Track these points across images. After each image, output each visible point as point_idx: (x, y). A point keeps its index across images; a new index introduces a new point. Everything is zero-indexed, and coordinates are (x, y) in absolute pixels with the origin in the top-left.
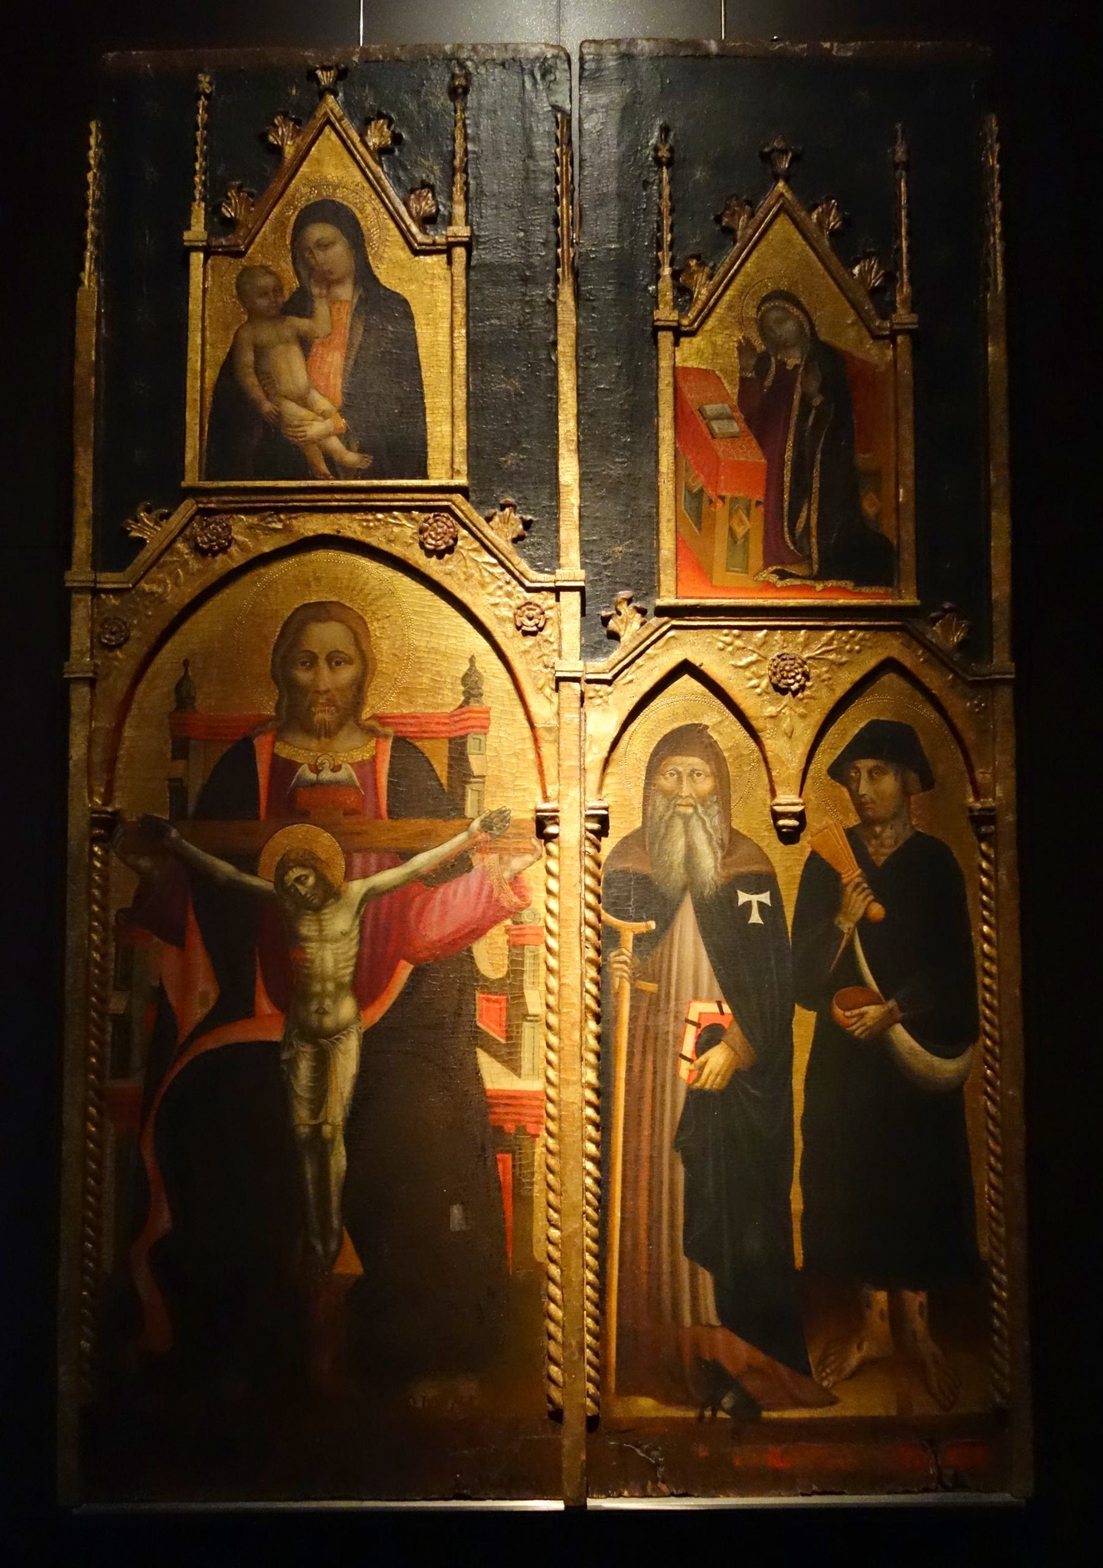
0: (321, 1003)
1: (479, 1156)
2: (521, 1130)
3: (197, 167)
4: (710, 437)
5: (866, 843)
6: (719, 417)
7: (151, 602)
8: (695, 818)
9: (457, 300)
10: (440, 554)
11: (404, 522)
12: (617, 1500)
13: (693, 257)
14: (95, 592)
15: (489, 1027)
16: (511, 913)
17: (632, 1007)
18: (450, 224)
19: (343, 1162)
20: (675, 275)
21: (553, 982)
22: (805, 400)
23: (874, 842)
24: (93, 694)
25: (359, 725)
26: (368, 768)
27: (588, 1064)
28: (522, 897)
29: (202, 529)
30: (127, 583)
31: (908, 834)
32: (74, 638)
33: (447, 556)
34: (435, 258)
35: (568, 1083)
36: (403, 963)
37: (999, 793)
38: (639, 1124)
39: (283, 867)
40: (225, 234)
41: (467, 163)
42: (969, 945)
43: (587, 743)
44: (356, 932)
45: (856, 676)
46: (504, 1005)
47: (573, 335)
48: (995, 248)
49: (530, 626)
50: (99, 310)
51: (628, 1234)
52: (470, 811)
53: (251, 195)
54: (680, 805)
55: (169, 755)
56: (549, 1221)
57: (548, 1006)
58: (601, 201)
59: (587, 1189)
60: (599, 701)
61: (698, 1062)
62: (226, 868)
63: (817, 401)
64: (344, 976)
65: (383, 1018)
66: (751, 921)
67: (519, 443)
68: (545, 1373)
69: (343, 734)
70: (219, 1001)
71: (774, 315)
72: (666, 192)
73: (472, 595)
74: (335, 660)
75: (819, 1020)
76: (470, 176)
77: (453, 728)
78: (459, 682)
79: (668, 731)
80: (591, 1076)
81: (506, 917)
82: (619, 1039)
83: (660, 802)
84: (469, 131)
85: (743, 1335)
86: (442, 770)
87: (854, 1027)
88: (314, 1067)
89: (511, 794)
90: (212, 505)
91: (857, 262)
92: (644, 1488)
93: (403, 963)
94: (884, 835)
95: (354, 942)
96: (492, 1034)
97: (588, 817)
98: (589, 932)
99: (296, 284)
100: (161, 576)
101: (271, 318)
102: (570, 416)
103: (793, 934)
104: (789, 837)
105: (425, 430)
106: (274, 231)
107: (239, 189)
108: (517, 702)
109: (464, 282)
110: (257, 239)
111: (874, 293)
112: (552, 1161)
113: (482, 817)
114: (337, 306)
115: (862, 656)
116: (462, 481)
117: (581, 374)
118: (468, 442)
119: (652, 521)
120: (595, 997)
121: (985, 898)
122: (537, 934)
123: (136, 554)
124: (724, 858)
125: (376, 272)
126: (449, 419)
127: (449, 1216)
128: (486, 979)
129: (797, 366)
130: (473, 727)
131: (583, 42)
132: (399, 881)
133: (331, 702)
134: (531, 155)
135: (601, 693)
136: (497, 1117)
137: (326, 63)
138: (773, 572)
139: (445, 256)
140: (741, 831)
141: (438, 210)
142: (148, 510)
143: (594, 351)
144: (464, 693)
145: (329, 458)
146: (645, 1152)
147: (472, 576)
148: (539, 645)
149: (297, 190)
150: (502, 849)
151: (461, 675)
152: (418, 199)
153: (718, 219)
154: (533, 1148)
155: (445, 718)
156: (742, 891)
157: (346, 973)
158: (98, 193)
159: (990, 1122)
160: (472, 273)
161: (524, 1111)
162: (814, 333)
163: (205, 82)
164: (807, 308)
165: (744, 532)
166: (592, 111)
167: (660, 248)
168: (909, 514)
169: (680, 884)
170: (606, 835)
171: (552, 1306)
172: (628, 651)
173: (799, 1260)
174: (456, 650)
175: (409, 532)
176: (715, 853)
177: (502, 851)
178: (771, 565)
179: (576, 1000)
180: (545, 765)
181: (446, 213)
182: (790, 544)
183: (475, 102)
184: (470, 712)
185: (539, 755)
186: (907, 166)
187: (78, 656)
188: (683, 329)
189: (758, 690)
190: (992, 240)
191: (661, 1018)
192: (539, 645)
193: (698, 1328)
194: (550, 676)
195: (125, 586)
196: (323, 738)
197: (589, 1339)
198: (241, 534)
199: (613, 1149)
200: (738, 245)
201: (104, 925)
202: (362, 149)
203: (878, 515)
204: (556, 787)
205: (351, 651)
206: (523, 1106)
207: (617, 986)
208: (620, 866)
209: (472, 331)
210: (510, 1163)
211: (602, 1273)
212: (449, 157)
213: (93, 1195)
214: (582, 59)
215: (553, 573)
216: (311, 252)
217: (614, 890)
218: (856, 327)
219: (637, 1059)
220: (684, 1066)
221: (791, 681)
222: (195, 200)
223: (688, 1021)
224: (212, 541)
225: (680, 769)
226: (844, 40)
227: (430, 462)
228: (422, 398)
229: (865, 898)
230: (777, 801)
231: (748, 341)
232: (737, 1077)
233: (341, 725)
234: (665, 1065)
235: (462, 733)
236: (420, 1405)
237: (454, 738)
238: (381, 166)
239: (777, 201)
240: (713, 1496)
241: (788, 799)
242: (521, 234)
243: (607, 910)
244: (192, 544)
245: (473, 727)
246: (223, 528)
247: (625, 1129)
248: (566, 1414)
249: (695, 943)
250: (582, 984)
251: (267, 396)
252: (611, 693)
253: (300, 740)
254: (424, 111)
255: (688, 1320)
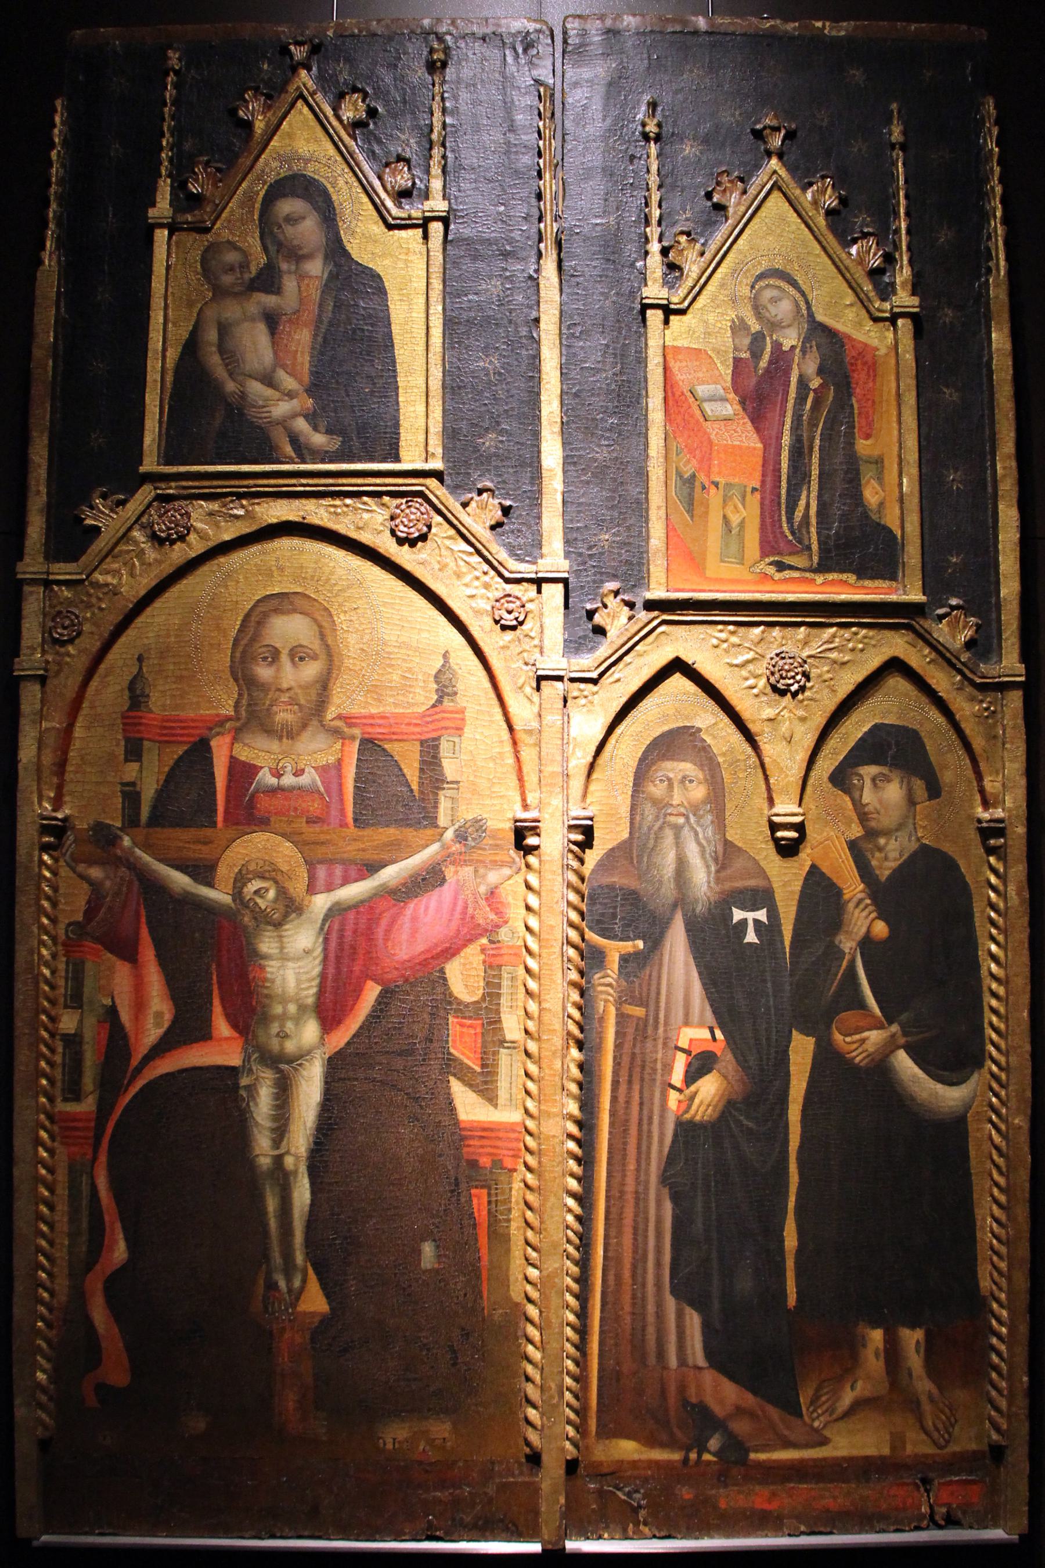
0: (282, 1026)
1: (452, 1191)
2: (498, 1163)
3: (164, 143)
4: (702, 420)
5: (870, 857)
6: (712, 399)
7: (105, 594)
8: (686, 829)
9: (433, 276)
10: (412, 543)
11: (374, 508)
12: (596, 1542)
13: (682, 233)
14: (47, 584)
15: (463, 1054)
16: (486, 931)
17: (617, 1033)
18: (427, 198)
19: (307, 1196)
20: (665, 252)
21: (533, 1007)
22: (803, 383)
23: (877, 854)
24: (43, 693)
25: (323, 726)
26: (333, 772)
27: (570, 1095)
28: (499, 913)
29: (160, 517)
30: (81, 574)
31: (914, 846)
32: (25, 633)
33: (420, 544)
34: (410, 232)
35: (549, 1115)
36: (370, 984)
37: (1008, 804)
38: (624, 1156)
39: (241, 880)
40: (190, 210)
41: (445, 137)
42: (976, 966)
43: (571, 746)
44: (319, 951)
45: (859, 677)
46: (479, 1030)
47: (557, 313)
48: (996, 232)
49: (509, 620)
50: (59, 288)
51: (611, 1278)
52: (443, 820)
53: (218, 170)
54: (670, 814)
55: (122, 757)
56: (527, 1259)
57: (527, 1032)
58: (587, 174)
59: (568, 1227)
60: (583, 701)
61: (688, 1092)
62: (180, 880)
63: (815, 383)
64: (306, 997)
65: (348, 1044)
66: (746, 941)
67: (498, 423)
68: (522, 1371)
69: (306, 735)
70: (175, 1022)
71: (768, 294)
72: (654, 168)
73: (447, 586)
74: (298, 655)
75: (818, 1044)
76: (448, 149)
77: (425, 729)
78: (432, 679)
79: (658, 734)
80: (573, 1108)
81: (481, 935)
82: (603, 1068)
83: (649, 812)
84: (448, 104)
85: (732, 1378)
86: (412, 775)
87: (854, 1054)
88: (273, 1093)
89: (488, 802)
90: (171, 491)
91: (854, 241)
92: (625, 1530)
93: (370, 984)
94: (889, 847)
95: (317, 961)
96: (466, 1061)
97: (571, 828)
98: (572, 952)
99: (263, 260)
100: (116, 566)
101: (236, 295)
102: (553, 396)
103: (790, 953)
104: (788, 850)
105: (398, 410)
106: (242, 205)
107: (207, 164)
108: (495, 702)
109: (441, 257)
110: (224, 215)
111: (875, 274)
112: (531, 1197)
113: (456, 826)
114: (306, 282)
115: (864, 656)
116: (437, 464)
117: (564, 352)
118: (444, 423)
119: (641, 508)
120: (577, 1023)
121: (993, 914)
122: (515, 954)
123: (91, 542)
124: (718, 871)
125: (348, 247)
126: (424, 398)
127: (420, 1254)
128: (460, 1002)
129: (793, 347)
130: (446, 728)
131: (566, 18)
132: (366, 895)
133: (293, 701)
134: (512, 129)
135: (585, 693)
136: (471, 1150)
137: (300, 38)
138: (771, 564)
139: (421, 230)
140: (736, 843)
141: (414, 183)
142: (104, 496)
143: (579, 329)
144: (437, 691)
145: (295, 440)
146: (630, 1187)
147: (446, 565)
148: (519, 640)
149: (266, 164)
150: (478, 861)
151: (434, 673)
152: (394, 174)
153: (709, 196)
154: (510, 1183)
155: (417, 718)
156: (737, 908)
157: (310, 994)
158: (61, 171)
159: (994, 1152)
160: (449, 248)
161: (499, 1143)
162: (811, 315)
163: (174, 58)
164: (804, 287)
165: (739, 520)
166: (576, 85)
167: (647, 223)
168: (913, 503)
169: (671, 900)
170: (591, 847)
171: (530, 1348)
172: (615, 647)
173: (792, 1300)
174: (429, 645)
175: (380, 519)
176: (708, 867)
177: (478, 864)
178: (767, 556)
179: (557, 1026)
180: (525, 770)
181: (423, 187)
182: (788, 533)
183: (454, 76)
184: (444, 712)
185: (518, 759)
186: (903, 147)
187: (28, 651)
188: (672, 306)
189: (755, 691)
190: (993, 223)
191: (649, 1044)
192: (519, 640)
193: (684, 1368)
194: (531, 674)
195: (78, 577)
196: (285, 740)
197: (568, 1381)
198: (201, 521)
199: (596, 1185)
200: (730, 221)
201: (54, 939)
202: (335, 123)
203: (881, 504)
204: (537, 795)
205: (316, 646)
206: (500, 1139)
207: (601, 1011)
208: (607, 880)
209: (448, 307)
210: (485, 1199)
211: (583, 1314)
212: (426, 130)
213: (46, 1223)
214: (565, 33)
215: (535, 563)
216: (280, 227)
217: (598, 906)
218: (854, 309)
219: (623, 1089)
220: (673, 1096)
221: (791, 681)
222: (161, 176)
223: (677, 1048)
224: (169, 529)
225: (671, 775)
226: (836, 19)
227: (402, 443)
228: (395, 377)
229: (867, 917)
230: (775, 810)
231: (742, 320)
232: (729, 1107)
233: (304, 726)
234: (652, 1095)
235: (434, 735)
236: (390, 1446)
237: (426, 741)
238: (355, 140)
239: (770, 178)
240: (697, 1538)
241: (786, 809)
242: (502, 208)
243: (591, 928)
244: (149, 531)
245: (446, 728)
246: (182, 515)
247: (609, 1163)
248: (545, 1458)
249: (686, 964)
250: (564, 1009)
251: (231, 375)
252: (597, 693)
253: (261, 742)
254: (399, 84)
255: (673, 1361)
